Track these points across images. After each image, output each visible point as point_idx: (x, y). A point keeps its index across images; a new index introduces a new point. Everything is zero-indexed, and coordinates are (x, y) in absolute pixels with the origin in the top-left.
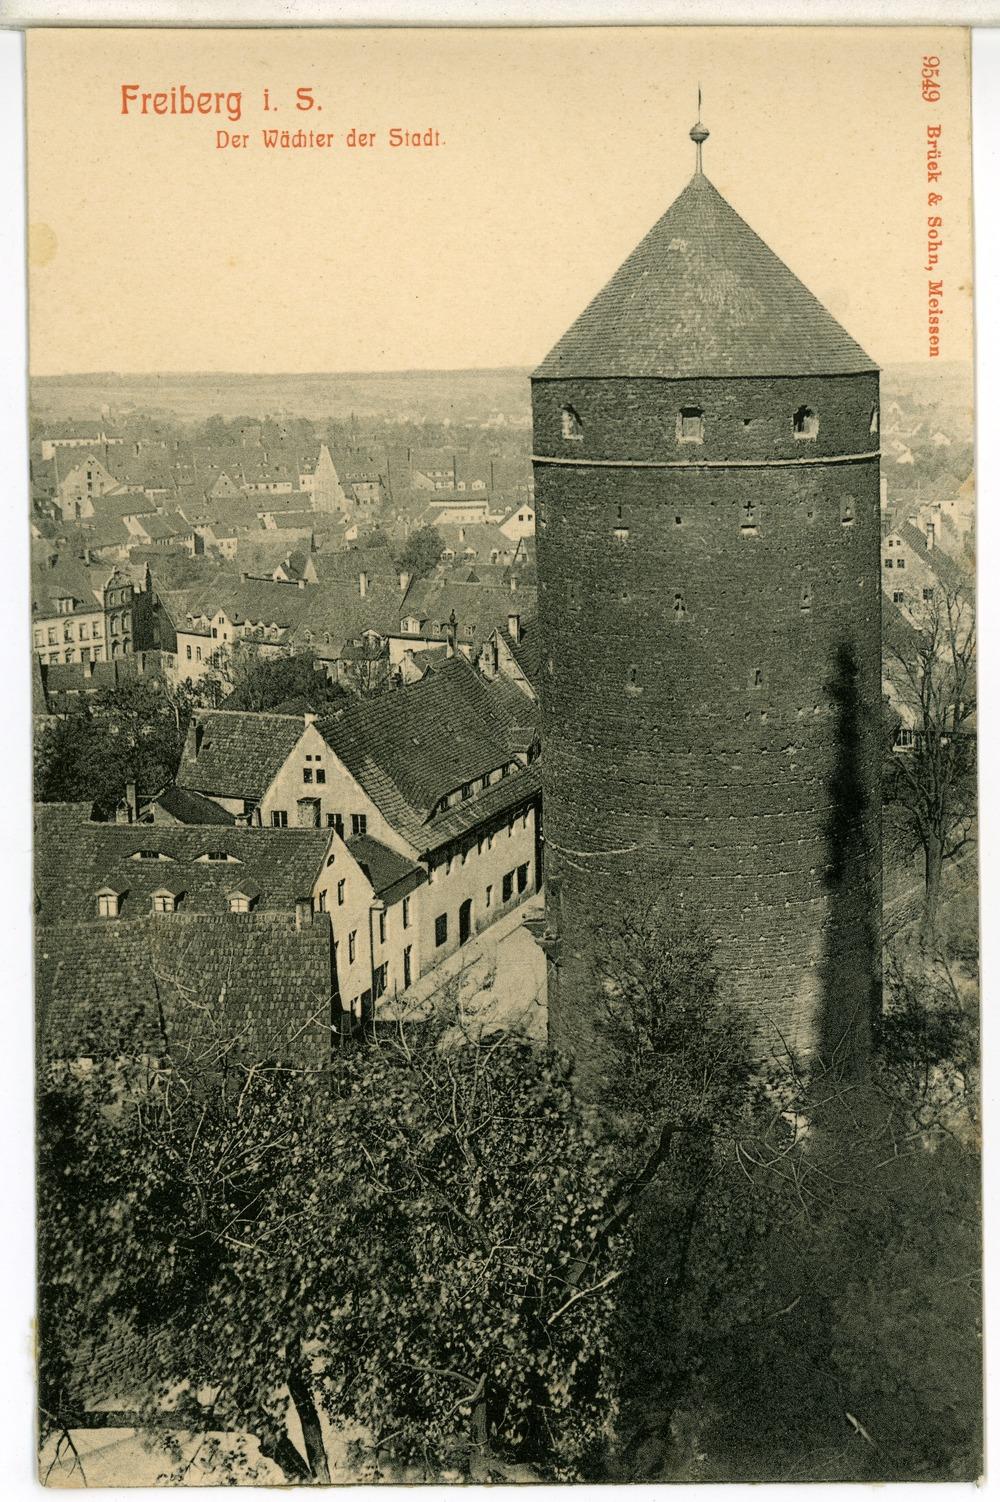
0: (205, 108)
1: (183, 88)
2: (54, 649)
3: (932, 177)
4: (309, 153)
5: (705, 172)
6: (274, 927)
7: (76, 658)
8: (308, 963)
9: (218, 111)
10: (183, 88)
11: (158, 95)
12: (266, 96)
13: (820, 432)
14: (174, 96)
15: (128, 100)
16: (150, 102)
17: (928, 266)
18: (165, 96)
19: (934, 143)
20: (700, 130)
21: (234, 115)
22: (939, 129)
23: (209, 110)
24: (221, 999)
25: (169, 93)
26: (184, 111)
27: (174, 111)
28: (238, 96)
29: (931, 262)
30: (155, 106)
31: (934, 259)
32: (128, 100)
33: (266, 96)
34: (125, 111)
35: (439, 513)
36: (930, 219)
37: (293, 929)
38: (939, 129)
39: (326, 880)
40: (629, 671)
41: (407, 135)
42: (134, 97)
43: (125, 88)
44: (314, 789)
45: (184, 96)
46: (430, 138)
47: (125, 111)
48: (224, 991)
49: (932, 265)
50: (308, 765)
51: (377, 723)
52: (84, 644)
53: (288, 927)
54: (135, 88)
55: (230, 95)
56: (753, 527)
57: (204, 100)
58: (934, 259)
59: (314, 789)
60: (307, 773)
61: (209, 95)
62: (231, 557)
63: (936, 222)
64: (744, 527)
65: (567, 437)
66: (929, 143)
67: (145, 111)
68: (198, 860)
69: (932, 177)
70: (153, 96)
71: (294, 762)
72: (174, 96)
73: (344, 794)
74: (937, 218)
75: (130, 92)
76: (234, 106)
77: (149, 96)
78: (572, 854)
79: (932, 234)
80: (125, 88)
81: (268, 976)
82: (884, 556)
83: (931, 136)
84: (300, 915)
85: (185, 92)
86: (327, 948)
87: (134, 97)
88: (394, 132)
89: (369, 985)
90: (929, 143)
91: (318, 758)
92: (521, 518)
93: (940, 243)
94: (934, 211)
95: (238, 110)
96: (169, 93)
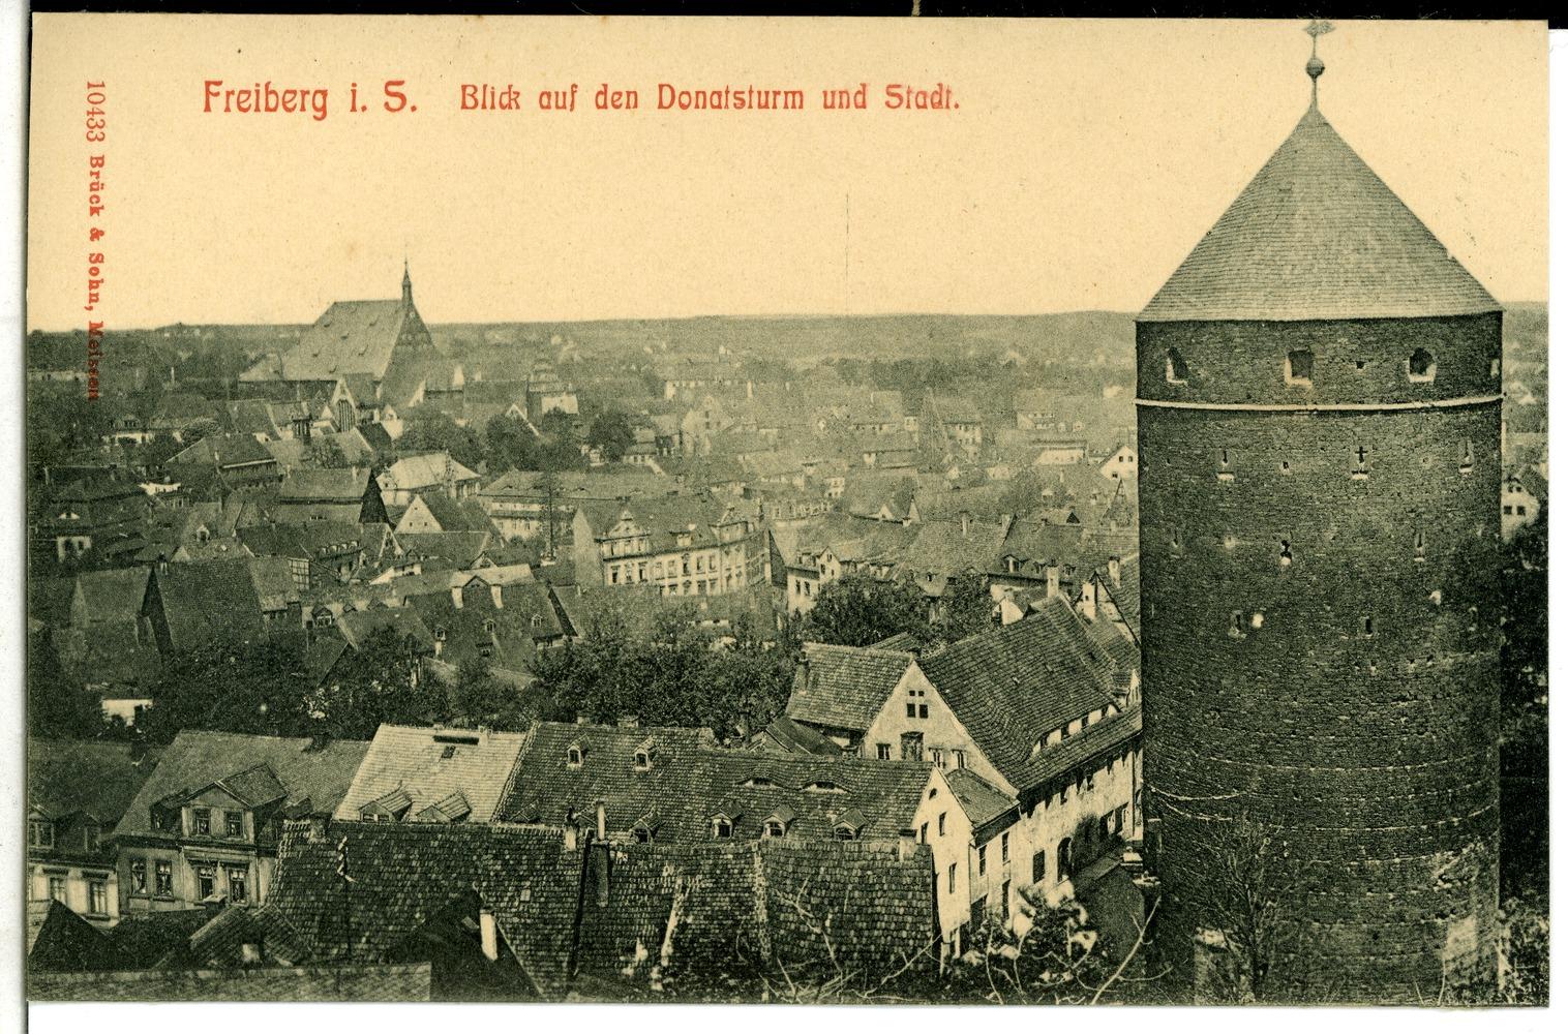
0: (290, 105)
1: (267, 85)
2: (673, 581)
3: (94, 211)
4: (780, 115)
5: (1320, 107)
6: (879, 857)
7: (694, 590)
8: (910, 895)
9: (303, 109)
10: (267, 85)
11: (241, 92)
12: (354, 92)
13: (1437, 376)
14: (258, 92)
15: (212, 98)
16: (233, 99)
17: (87, 305)
18: (248, 92)
19: (97, 174)
20: (1315, 63)
21: (319, 114)
22: (102, 158)
23: (293, 109)
24: (828, 923)
25: (253, 88)
26: (268, 109)
27: (257, 109)
28: (324, 93)
29: (91, 301)
30: (239, 103)
31: (94, 298)
32: (212, 98)
33: (354, 92)
34: (208, 109)
35: (1039, 454)
36: (92, 255)
37: (897, 860)
38: (102, 158)
39: (927, 811)
40: (1233, 617)
41: (909, 92)
42: (217, 94)
43: (208, 84)
44: (917, 724)
45: (268, 92)
46: (939, 99)
47: (208, 109)
48: (830, 916)
49: (93, 304)
50: (911, 700)
51: (979, 660)
52: (701, 577)
53: (892, 857)
54: (219, 83)
55: (316, 92)
56: (1365, 472)
57: (289, 97)
58: (94, 298)
59: (917, 724)
60: (911, 707)
61: (294, 92)
62: (839, 496)
63: (98, 258)
64: (1354, 473)
65: (1170, 380)
66: (92, 174)
67: (228, 109)
68: (808, 789)
69: (94, 211)
70: (237, 93)
71: (898, 697)
72: (258, 92)
73: (945, 728)
74: (100, 255)
75: (213, 89)
76: (319, 102)
77: (308, 92)
78: (1172, 798)
79: (94, 271)
80: (208, 84)
81: (873, 905)
82: (1504, 502)
83: (93, 166)
84: (906, 847)
85: (271, 88)
86: (929, 880)
87: (217, 94)
88: (891, 90)
89: (968, 917)
90: (92, 174)
91: (921, 694)
92: (1121, 459)
93: (102, 281)
94: (96, 247)
95: (324, 109)
96: (253, 88)
